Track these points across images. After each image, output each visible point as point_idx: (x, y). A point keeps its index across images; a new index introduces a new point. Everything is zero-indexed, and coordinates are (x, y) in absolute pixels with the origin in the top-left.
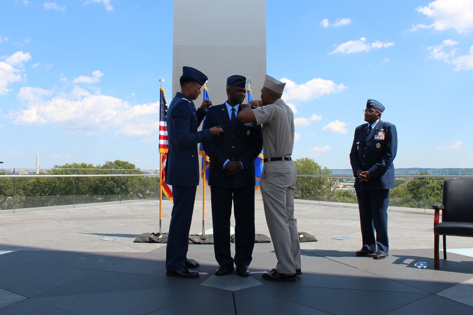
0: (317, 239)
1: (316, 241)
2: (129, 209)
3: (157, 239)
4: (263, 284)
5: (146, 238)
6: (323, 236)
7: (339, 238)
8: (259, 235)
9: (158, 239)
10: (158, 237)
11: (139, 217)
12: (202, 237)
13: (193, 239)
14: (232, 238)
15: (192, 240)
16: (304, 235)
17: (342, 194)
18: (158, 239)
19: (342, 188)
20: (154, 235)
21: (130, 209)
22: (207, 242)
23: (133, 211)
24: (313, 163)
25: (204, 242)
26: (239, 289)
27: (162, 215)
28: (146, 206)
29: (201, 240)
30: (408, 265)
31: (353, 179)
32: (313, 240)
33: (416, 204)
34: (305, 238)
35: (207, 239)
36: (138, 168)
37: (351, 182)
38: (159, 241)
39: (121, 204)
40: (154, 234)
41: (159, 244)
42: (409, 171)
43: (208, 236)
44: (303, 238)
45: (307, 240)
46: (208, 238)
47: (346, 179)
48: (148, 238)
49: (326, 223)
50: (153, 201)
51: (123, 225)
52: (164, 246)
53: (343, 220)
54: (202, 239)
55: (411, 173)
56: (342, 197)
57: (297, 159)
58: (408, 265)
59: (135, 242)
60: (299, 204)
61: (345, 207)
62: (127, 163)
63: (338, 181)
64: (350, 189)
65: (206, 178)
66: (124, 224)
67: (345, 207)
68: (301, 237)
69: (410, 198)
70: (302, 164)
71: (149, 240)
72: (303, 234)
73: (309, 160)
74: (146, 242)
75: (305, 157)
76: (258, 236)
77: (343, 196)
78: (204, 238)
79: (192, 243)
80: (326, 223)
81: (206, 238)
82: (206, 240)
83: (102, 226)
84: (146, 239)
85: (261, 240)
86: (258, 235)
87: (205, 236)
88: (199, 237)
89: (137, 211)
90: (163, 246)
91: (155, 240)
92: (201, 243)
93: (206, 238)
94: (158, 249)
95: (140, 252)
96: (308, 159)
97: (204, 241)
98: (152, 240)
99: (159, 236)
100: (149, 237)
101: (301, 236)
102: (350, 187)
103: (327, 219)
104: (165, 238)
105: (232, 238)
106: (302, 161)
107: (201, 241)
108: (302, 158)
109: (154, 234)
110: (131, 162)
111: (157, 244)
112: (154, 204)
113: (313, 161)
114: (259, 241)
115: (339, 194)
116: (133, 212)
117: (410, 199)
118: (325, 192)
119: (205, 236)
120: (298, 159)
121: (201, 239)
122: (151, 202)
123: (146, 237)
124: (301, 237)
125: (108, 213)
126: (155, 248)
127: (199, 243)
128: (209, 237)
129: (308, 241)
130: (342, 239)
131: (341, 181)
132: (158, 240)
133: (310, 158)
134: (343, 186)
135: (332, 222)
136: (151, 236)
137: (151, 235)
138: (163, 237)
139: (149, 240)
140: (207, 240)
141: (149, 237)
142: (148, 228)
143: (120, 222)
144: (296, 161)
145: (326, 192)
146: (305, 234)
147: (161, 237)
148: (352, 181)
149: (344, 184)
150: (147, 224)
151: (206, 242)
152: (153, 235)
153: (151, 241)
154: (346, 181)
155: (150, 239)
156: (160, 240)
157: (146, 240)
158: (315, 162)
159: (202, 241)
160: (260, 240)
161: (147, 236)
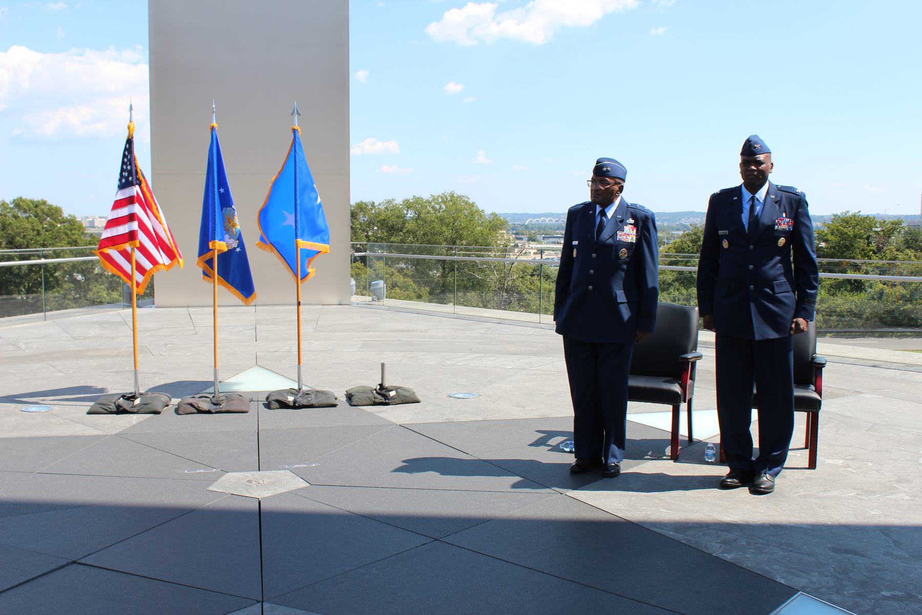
0: (420, 398)
1: (419, 402)
2: (68, 335)
3: (131, 405)
4: (309, 485)
5: (111, 405)
6: (433, 391)
7: (460, 396)
8: (318, 393)
9: (132, 407)
10: (132, 403)
11: (90, 354)
12: (214, 400)
13: (198, 404)
14: (269, 400)
15: (196, 405)
16: (396, 392)
17: (530, 271)
18: (132, 407)
19: (534, 256)
20: (125, 399)
21: (68, 333)
22: (223, 410)
23: (75, 339)
24: (467, 203)
25: (218, 408)
26: (270, 495)
27: (137, 348)
28: (101, 324)
29: (212, 404)
30: (551, 448)
31: (558, 235)
32: (412, 401)
33: (682, 294)
34: (399, 397)
35: (223, 403)
36: (70, 215)
37: (554, 243)
38: (135, 410)
39: (47, 322)
40: (125, 398)
41: (134, 417)
42: (677, 219)
43: (224, 398)
44: (395, 397)
45: (402, 401)
46: (224, 401)
47: (543, 236)
48: (113, 404)
49: (449, 362)
50: (115, 312)
51: (60, 374)
52: (145, 419)
53: (483, 355)
54: (215, 404)
55: (682, 224)
56: (529, 277)
57: (431, 195)
58: (551, 448)
59: (89, 413)
60: (413, 315)
61: (500, 322)
62: (44, 203)
63: (525, 238)
64: (552, 258)
65: (218, 273)
66: (63, 374)
67: (500, 322)
68: (391, 396)
69: (672, 280)
70: (443, 206)
71: (115, 409)
72: (396, 389)
73: (458, 197)
74: (111, 413)
75: (448, 191)
76: (316, 395)
77: (532, 275)
78: (218, 401)
79: (196, 411)
80: (449, 362)
81: (221, 402)
82: (221, 405)
83: (18, 378)
84: (111, 407)
85: (320, 403)
86: (315, 393)
87: (219, 398)
88: (208, 399)
89: (83, 339)
90: (142, 420)
91: (128, 409)
92: (212, 411)
93: (222, 401)
94: (134, 426)
95: (101, 433)
96: (455, 195)
97: (218, 406)
98: (122, 408)
99: (134, 401)
100: (116, 403)
101: (392, 394)
102: (551, 252)
103: (455, 353)
104: (145, 404)
105: (269, 400)
106: (443, 200)
107: (213, 408)
108: (443, 194)
109: (125, 398)
110: (53, 201)
111: (132, 415)
112: (119, 319)
113: (466, 200)
114: (317, 405)
115: (524, 272)
116: (76, 342)
117: (670, 282)
118: (493, 267)
119: (219, 398)
120: (433, 195)
121: (212, 403)
122: (111, 313)
123: (111, 404)
124: (391, 396)
125: (24, 346)
126: (128, 425)
127: (209, 412)
128: (227, 399)
129: (404, 402)
130: (466, 396)
131: (532, 239)
132: (133, 409)
133: (458, 192)
134: (535, 251)
135: (461, 359)
136: (119, 400)
137: (119, 398)
138: (144, 403)
139: (115, 409)
140: (223, 405)
141: (115, 403)
142: (111, 380)
143: (53, 369)
144: (431, 199)
145: (494, 267)
146: (399, 390)
147: (137, 401)
148: (557, 240)
149: (539, 246)
150: (109, 372)
151: (221, 409)
152: (123, 398)
153: (120, 411)
154: (543, 239)
155: (118, 406)
156: (136, 408)
157: (109, 408)
158: (471, 201)
159: (215, 406)
160: (318, 402)
161: (112, 402)
